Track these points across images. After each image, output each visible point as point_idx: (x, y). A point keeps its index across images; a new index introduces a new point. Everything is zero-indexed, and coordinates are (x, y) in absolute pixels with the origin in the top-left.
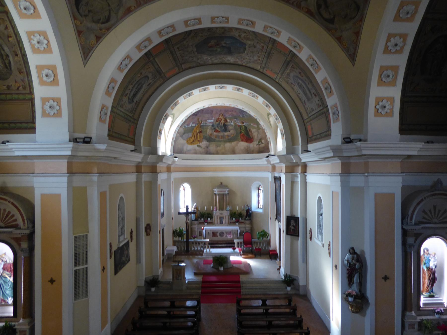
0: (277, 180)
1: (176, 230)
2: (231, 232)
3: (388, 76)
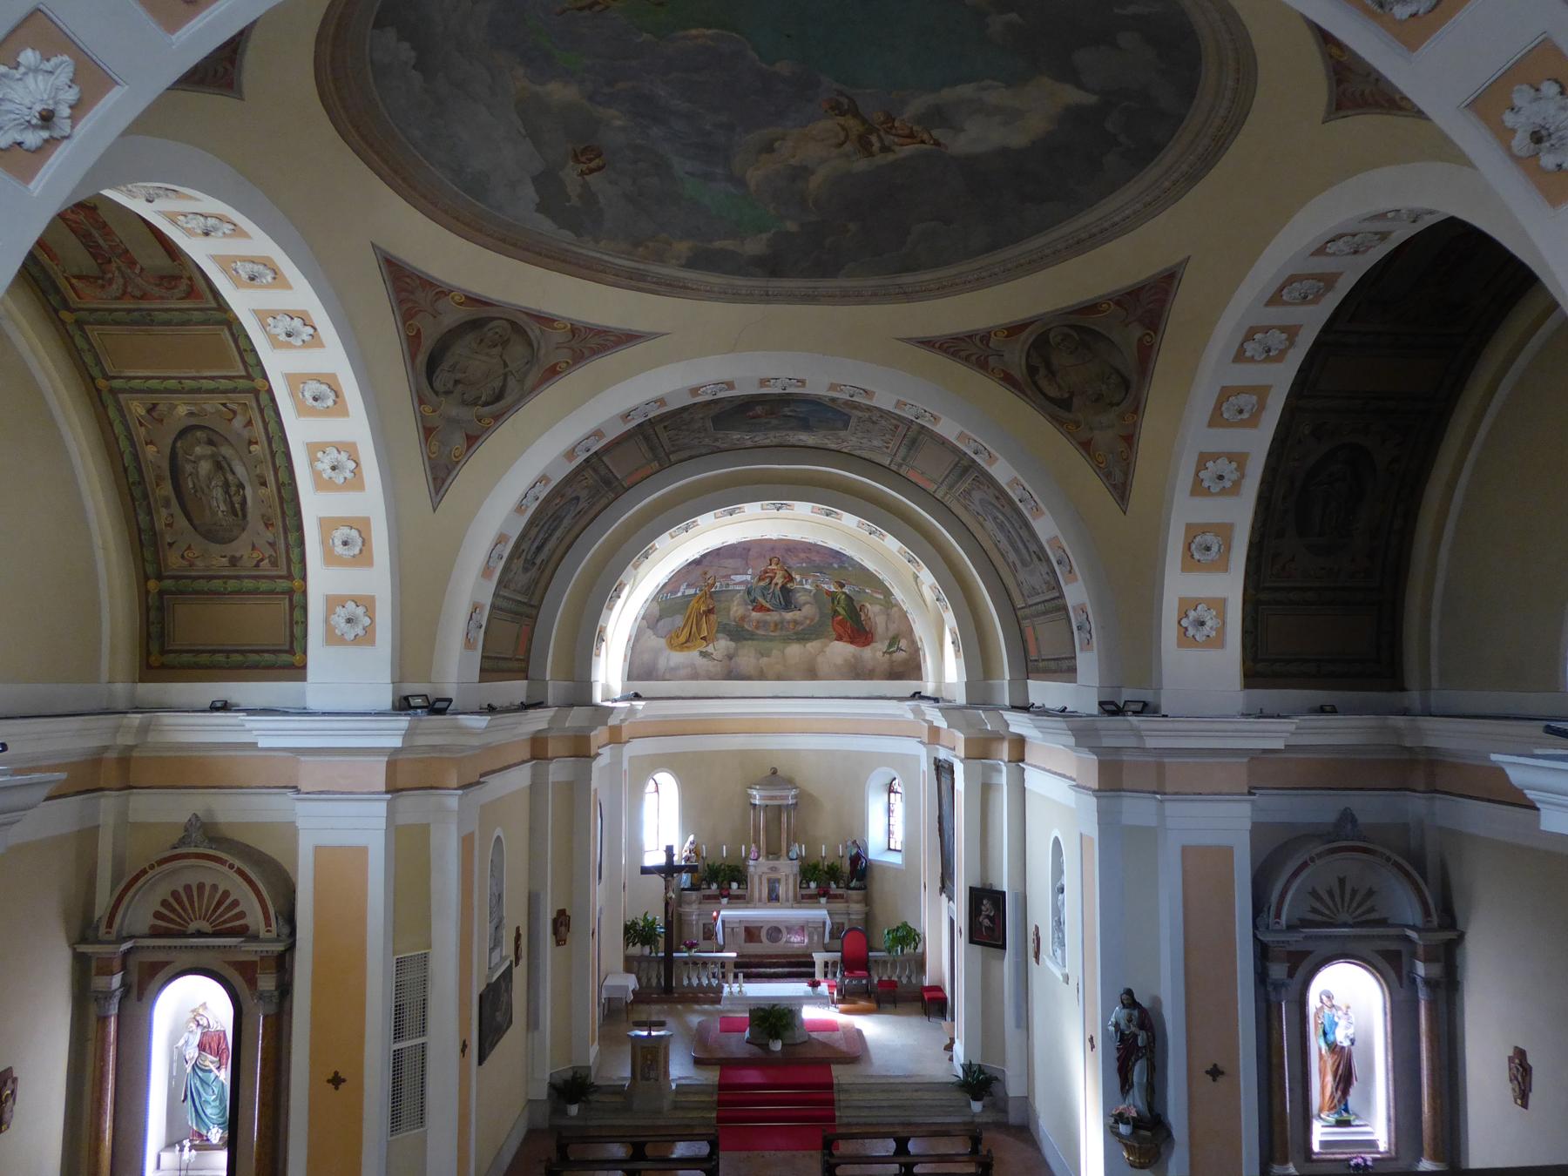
0: (943, 770)
1: (634, 924)
2: (802, 928)
3: (1208, 549)
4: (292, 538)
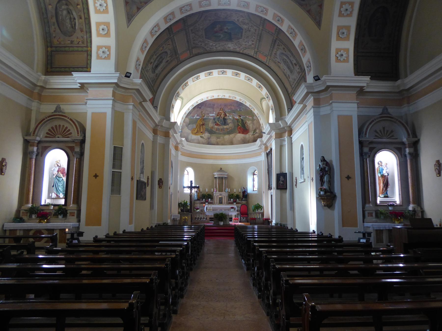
3: (343, 33)
4: (88, 35)
